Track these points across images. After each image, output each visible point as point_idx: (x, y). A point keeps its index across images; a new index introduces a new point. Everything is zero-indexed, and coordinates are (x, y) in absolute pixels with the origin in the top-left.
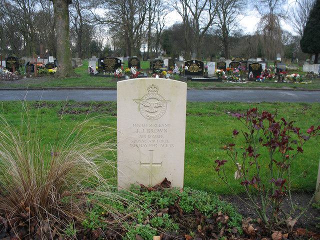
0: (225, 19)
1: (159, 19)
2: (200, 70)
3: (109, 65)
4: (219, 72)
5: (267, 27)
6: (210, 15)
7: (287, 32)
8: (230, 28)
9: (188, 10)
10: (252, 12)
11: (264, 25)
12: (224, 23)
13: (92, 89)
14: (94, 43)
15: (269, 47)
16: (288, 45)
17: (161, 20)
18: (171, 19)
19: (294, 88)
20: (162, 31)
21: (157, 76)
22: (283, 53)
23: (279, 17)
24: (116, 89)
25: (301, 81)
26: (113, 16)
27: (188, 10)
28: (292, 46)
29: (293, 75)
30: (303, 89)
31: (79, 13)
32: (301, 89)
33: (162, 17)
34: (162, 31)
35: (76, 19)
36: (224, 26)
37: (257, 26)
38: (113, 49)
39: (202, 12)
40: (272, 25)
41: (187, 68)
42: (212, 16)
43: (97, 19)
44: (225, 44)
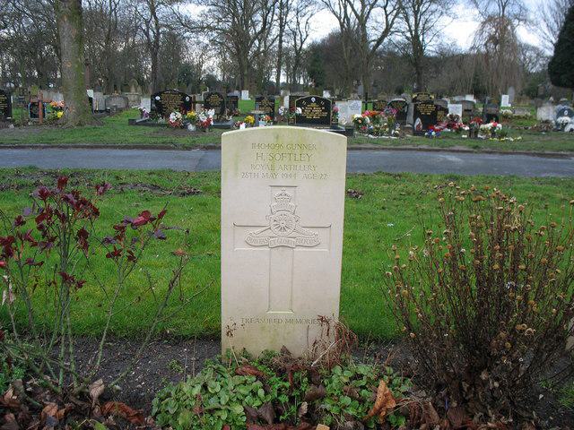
0: (417, 25)
1: (298, 23)
2: (325, 114)
3: (227, 109)
4: (359, 119)
5: (492, 38)
6: (387, 16)
7: (534, 49)
8: (427, 41)
9: (349, 9)
10: (467, 11)
11: (486, 35)
12: (416, 30)
13: (101, 147)
14: (188, 66)
15: (495, 75)
16: (537, 73)
17: (302, 26)
18: (320, 26)
19: (475, 147)
20: (305, 46)
21: (243, 126)
22: (519, 89)
23: (516, 22)
24: (220, 148)
25: (503, 134)
26: (214, 17)
27: (349, 9)
28: (539, 77)
29: (490, 125)
30: (92, 144)
31: (153, 13)
32: (488, 149)
33: (305, 19)
34: (305, 46)
35: (147, 22)
36: (417, 37)
37: (471, 39)
38: (220, 78)
39: (373, 11)
40: (501, 31)
41: (299, 110)
42: (390, 18)
43: (188, 25)
44: (416, 65)
